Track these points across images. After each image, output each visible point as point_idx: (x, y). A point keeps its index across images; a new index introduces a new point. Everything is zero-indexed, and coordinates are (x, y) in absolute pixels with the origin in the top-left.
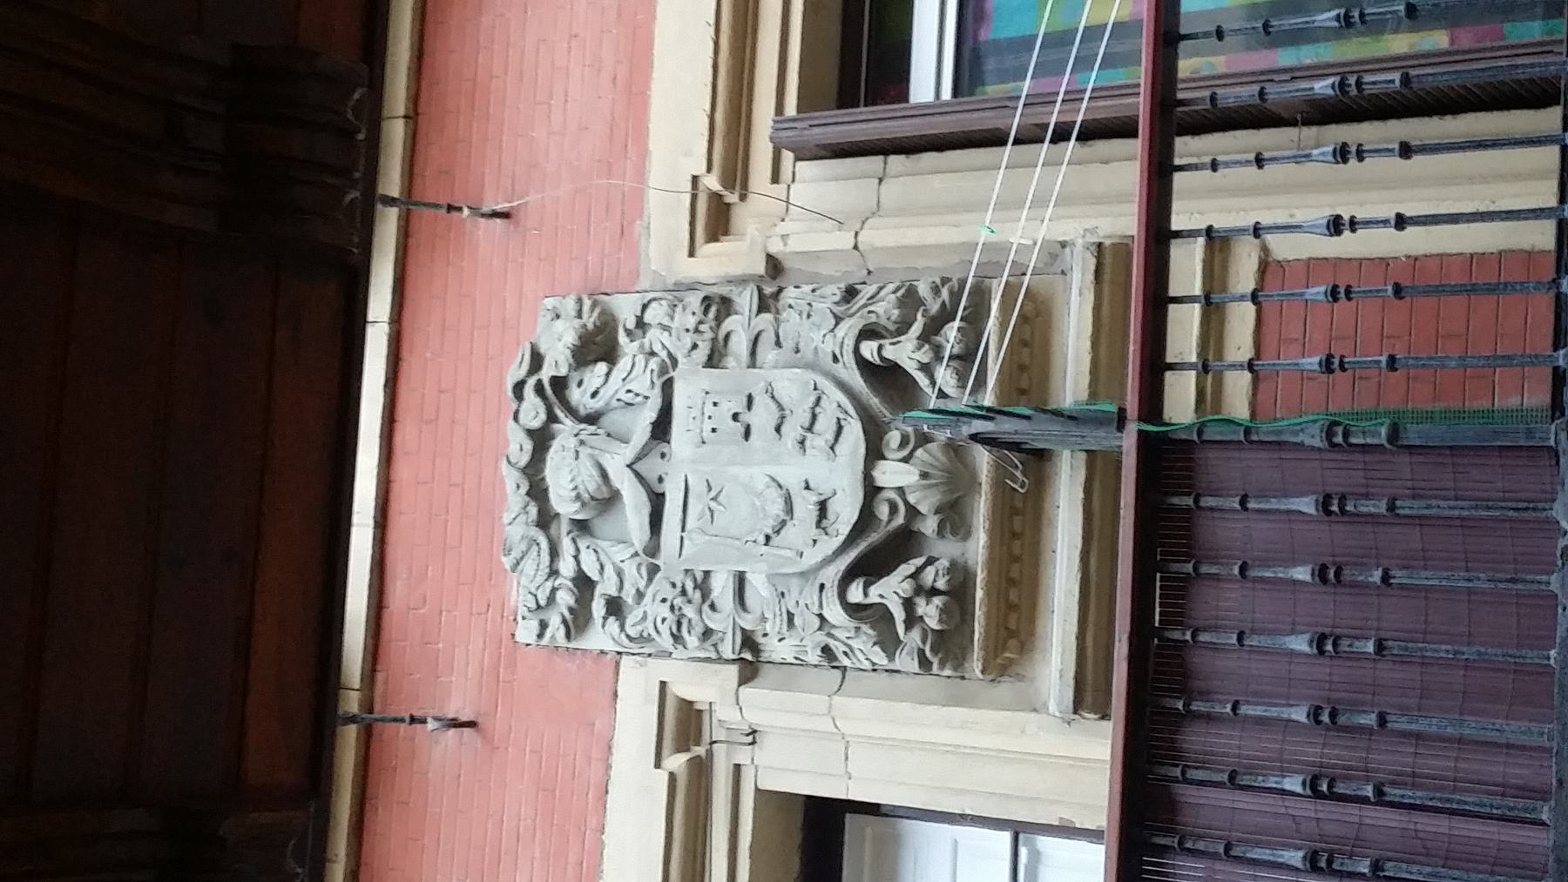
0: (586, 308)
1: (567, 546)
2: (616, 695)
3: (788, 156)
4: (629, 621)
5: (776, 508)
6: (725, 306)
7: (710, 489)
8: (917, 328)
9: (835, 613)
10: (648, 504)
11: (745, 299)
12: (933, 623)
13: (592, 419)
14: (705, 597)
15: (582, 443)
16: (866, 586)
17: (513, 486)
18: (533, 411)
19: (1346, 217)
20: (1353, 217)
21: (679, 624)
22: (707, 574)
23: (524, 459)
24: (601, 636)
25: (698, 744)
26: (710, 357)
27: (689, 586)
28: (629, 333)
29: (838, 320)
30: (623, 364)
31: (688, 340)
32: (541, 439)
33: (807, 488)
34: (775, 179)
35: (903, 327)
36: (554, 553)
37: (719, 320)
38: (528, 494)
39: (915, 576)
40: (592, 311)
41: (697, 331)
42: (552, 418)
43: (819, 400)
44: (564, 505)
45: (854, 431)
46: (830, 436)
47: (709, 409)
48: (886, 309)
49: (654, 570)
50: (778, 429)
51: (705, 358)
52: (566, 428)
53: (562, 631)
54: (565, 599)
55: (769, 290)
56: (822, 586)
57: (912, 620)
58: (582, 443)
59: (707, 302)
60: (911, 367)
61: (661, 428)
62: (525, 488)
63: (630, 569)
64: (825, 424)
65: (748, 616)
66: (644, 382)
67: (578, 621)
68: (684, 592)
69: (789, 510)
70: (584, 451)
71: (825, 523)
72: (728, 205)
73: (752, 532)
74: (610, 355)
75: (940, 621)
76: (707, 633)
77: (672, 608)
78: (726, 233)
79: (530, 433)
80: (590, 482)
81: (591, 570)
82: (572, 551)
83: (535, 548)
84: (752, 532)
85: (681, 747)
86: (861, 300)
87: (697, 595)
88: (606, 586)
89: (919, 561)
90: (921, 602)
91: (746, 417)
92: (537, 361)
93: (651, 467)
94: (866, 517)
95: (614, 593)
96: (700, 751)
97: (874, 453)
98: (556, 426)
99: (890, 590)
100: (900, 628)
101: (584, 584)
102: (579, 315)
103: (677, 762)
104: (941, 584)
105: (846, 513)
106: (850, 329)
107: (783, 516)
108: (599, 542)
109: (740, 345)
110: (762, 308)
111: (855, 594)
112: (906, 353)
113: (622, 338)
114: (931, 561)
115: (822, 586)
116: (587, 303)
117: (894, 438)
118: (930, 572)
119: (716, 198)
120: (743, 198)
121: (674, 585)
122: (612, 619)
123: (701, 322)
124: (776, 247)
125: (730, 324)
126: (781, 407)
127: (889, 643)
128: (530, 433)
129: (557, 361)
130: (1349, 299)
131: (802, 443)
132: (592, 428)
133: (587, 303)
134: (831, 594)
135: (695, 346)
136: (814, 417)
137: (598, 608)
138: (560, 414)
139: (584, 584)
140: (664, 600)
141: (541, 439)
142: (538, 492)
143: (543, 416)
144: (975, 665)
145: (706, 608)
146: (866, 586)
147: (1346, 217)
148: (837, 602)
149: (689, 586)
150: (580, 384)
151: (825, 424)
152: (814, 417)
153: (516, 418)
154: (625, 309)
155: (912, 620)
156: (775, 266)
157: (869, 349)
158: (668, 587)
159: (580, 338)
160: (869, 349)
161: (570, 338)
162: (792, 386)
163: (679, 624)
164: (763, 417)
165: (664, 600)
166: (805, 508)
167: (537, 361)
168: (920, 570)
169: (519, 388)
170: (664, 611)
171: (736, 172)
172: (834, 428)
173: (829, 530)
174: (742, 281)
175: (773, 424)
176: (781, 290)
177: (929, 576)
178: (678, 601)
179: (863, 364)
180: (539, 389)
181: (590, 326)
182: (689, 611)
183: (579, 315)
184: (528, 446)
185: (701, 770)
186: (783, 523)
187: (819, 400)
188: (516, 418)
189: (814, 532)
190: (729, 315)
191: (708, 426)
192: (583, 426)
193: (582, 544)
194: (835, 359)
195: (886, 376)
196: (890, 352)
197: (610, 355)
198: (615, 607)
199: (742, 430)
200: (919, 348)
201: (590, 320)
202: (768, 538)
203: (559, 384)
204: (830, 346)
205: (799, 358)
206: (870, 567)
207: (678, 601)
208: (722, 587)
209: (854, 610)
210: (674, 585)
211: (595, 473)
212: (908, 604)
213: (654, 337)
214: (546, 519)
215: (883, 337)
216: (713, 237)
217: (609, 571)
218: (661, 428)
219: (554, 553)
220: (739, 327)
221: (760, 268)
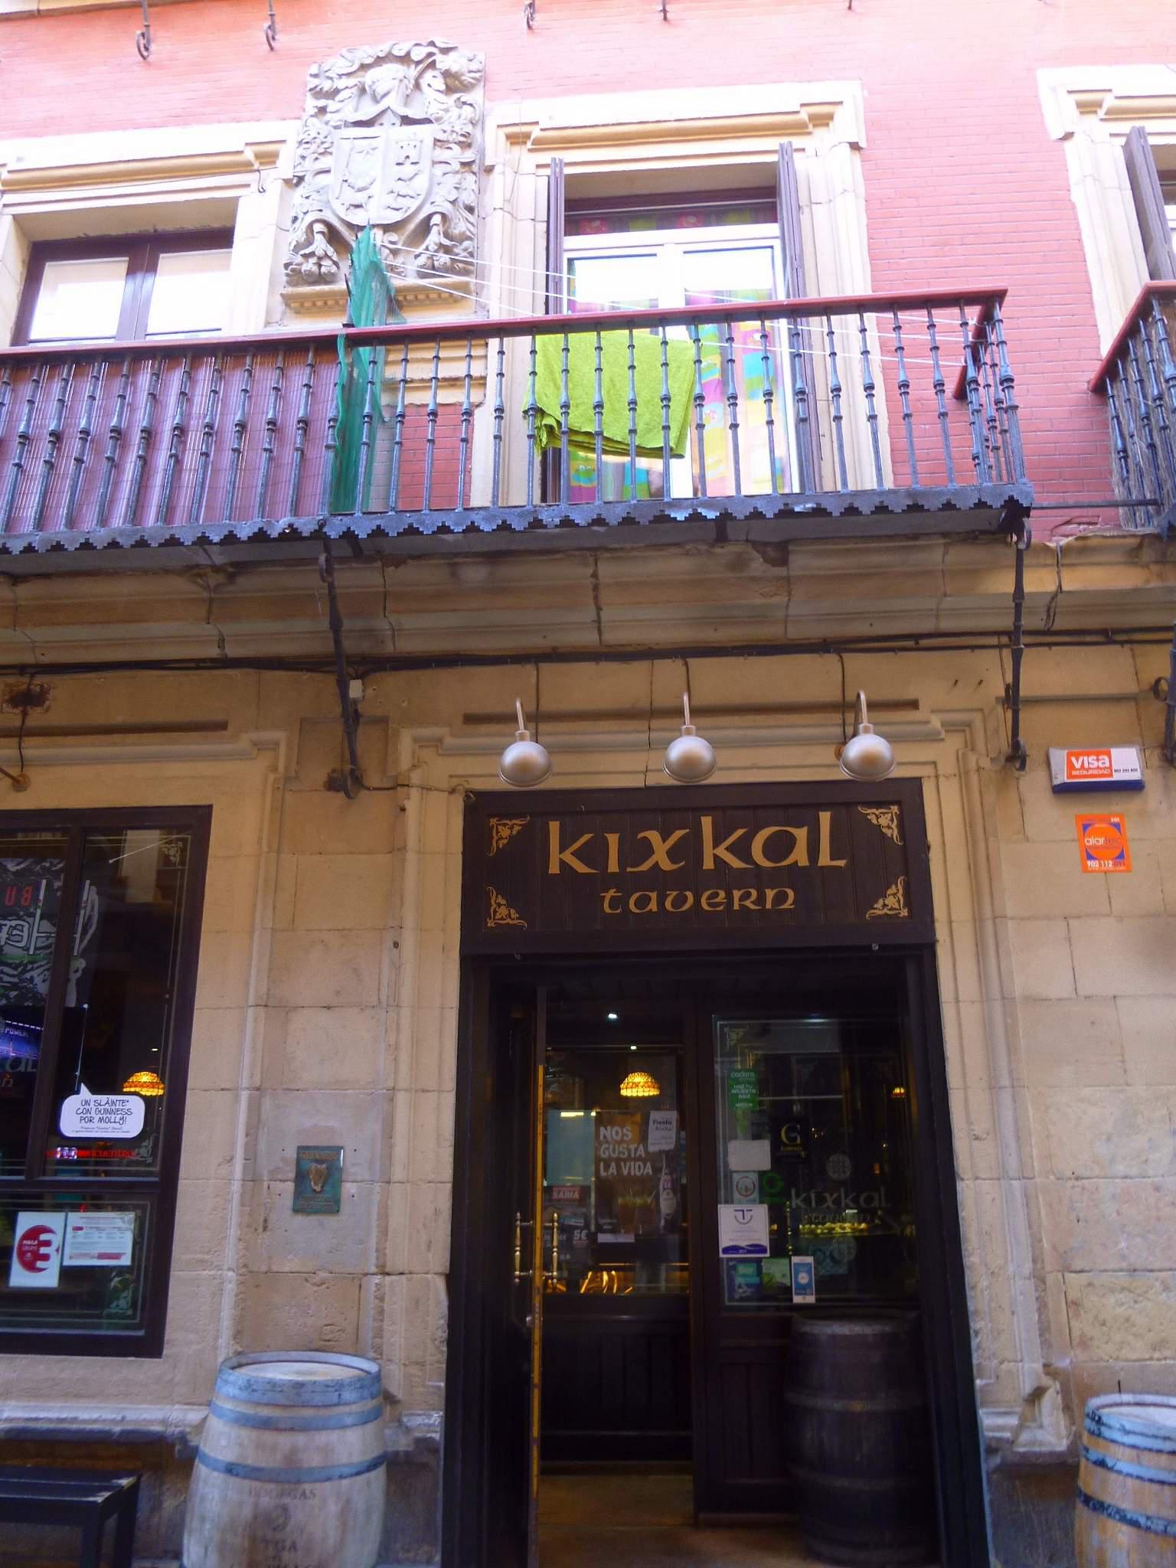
0: (473, 75)
1: (352, 81)
2: (285, 119)
3: (548, 171)
4: (314, 120)
5: (360, 184)
6: (465, 145)
7: (373, 149)
8: (447, 242)
9: (309, 218)
10: (368, 118)
11: (469, 155)
12: (304, 268)
13: (417, 86)
14: (321, 154)
15: (401, 81)
16: (322, 233)
17: (382, 50)
18: (418, 54)
19: (874, 392)
20: (873, 395)
21: (307, 143)
22: (331, 153)
23: (396, 52)
24: (311, 104)
25: (261, 164)
26: (439, 141)
27: (326, 145)
28: (459, 99)
29: (453, 202)
30: (442, 97)
31: (448, 128)
32: (405, 59)
33: (370, 197)
34: (538, 166)
35: (447, 235)
36: (349, 75)
37: (460, 143)
38: (378, 57)
39: (326, 255)
40: (473, 78)
41: (453, 131)
42: (418, 63)
43: (412, 197)
44: (369, 77)
45: (397, 217)
46: (394, 206)
47: (413, 144)
48: (460, 227)
49: (336, 127)
50: (399, 179)
51: (438, 138)
52: (413, 72)
53: (312, 86)
54: (327, 85)
55: (475, 168)
56: (321, 211)
57: (306, 256)
58: (401, 81)
59: (467, 135)
60: (427, 242)
61: (407, 121)
62: (381, 55)
63: (337, 116)
64: (402, 202)
65: (311, 178)
66: (433, 111)
67: (318, 93)
68: (323, 143)
69: (360, 190)
70: (396, 82)
71: (352, 208)
72: (526, 143)
73: (350, 173)
74: (449, 90)
75: (305, 271)
76: (303, 158)
77: (315, 138)
78: (512, 144)
79: (408, 54)
80: (380, 90)
81: (340, 97)
82: (350, 85)
83: (350, 64)
84: (350, 173)
85: (258, 156)
86: (467, 214)
87: (322, 150)
88: (332, 105)
89: (335, 258)
90: (314, 260)
91: (408, 161)
92: (446, 51)
93: (388, 118)
94: (356, 228)
95: (328, 110)
96: (256, 166)
97: (387, 228)
98: (413, 66)
99: (320, 245)
100: (302, 252)
101: (333, 93)
102: (470, 72)
103: (249, 155)
104: (323, 269)
105: (358, 218)
106: (447, 208)
107: (356, 187)
108: (356, 99)
109: (445, 155)
110: (463, 164)
111: (318, 227)
112: (434, 237)
113: (456, 96)
114: (335, 263)
115: (321, 211)
116: (477, 75)
117: (394, 237)
118: (329, 263)
119: (527, 136)
120: (530, 150)
121: (326, 137)
122: (316, 110)
123: (457, 133)
124: (497, 170)
125: (456, 148)
126: (411, 179)
127: (297, 248)
128: (408, 54)
129: (444, 62)
130: (901, 394)
131: (392, 192)
132: (411, 86)
133: (477, 75)
134: (318, 215)
135: (445, 132)
136: (404, 196)
137: (322, 103)
138: (421, 67)
139: (333, 93)
140: (319, 133)
141: (405, 59)
142: (379, 61)
143: (416, 60)
144: (290, 290)
145: (316, 155)
146: (322, 233)
147: (874, 392)
148: (313, 219)
149: (326, 145)
150: (434, 77)
151: (402, 202)
152: (404, 196)
153: (417, 45)
154: (475, 96)
155: (306, 256)
156: (490, 170)
157: (436, 219)
158: (325, 135)
159: (456, 73)
160: (436, 219)
161: (454, 69)
162: (421, 184)
163: (307, 143)
164: (408, 170)
165: (319, 133)
166: (360, 198)
167: (446, 51)
168: (330, 258)
169: (432, 44)
170: (313, 134)
171: (541, 145)
172: (398, 207)
173: (349, 211)
174: (482, 153)
175: (402, 177)
176: (474, 173)
177: (326, 263)
178: (318, 141)
179: (430, 217)
180: (430, 55)
181: (463, 78)
182: (313, 147)
183: (470, 72)
184: (402, 53)
185: (246, 167)
186: (353, 188)
187: (412, 197)
188: (417, 45)
189: (347, 204)
190: (461, 148)
191: (404, 144)
192: (413, 82)
193: (354, 90)
194: (432, 203)
195: (425, 228)
196: (435, 230)
197: (449, 90)
198: (322, 110)
199: (400, 162)
200: (435, 244)
201: (467, 78)
202: (346, 181)
203: (433, 65)
204: (438, 199)
205: (432, 183)
206: (333, 235)
207: (318, 141)
208: (325, 162)
209: (310, 226)
210: (326, 137)
211: (385, 91)
212: (312, 254)
213: (455, 111)
214: (364, 67)
215: (444, 225)
216: (508, 137)
217: (340, 105)
218: (407, 121)
219: (349, 75)
220: (455, 155)
221: (488, 163)
